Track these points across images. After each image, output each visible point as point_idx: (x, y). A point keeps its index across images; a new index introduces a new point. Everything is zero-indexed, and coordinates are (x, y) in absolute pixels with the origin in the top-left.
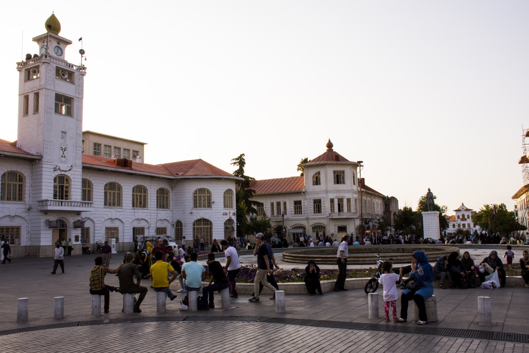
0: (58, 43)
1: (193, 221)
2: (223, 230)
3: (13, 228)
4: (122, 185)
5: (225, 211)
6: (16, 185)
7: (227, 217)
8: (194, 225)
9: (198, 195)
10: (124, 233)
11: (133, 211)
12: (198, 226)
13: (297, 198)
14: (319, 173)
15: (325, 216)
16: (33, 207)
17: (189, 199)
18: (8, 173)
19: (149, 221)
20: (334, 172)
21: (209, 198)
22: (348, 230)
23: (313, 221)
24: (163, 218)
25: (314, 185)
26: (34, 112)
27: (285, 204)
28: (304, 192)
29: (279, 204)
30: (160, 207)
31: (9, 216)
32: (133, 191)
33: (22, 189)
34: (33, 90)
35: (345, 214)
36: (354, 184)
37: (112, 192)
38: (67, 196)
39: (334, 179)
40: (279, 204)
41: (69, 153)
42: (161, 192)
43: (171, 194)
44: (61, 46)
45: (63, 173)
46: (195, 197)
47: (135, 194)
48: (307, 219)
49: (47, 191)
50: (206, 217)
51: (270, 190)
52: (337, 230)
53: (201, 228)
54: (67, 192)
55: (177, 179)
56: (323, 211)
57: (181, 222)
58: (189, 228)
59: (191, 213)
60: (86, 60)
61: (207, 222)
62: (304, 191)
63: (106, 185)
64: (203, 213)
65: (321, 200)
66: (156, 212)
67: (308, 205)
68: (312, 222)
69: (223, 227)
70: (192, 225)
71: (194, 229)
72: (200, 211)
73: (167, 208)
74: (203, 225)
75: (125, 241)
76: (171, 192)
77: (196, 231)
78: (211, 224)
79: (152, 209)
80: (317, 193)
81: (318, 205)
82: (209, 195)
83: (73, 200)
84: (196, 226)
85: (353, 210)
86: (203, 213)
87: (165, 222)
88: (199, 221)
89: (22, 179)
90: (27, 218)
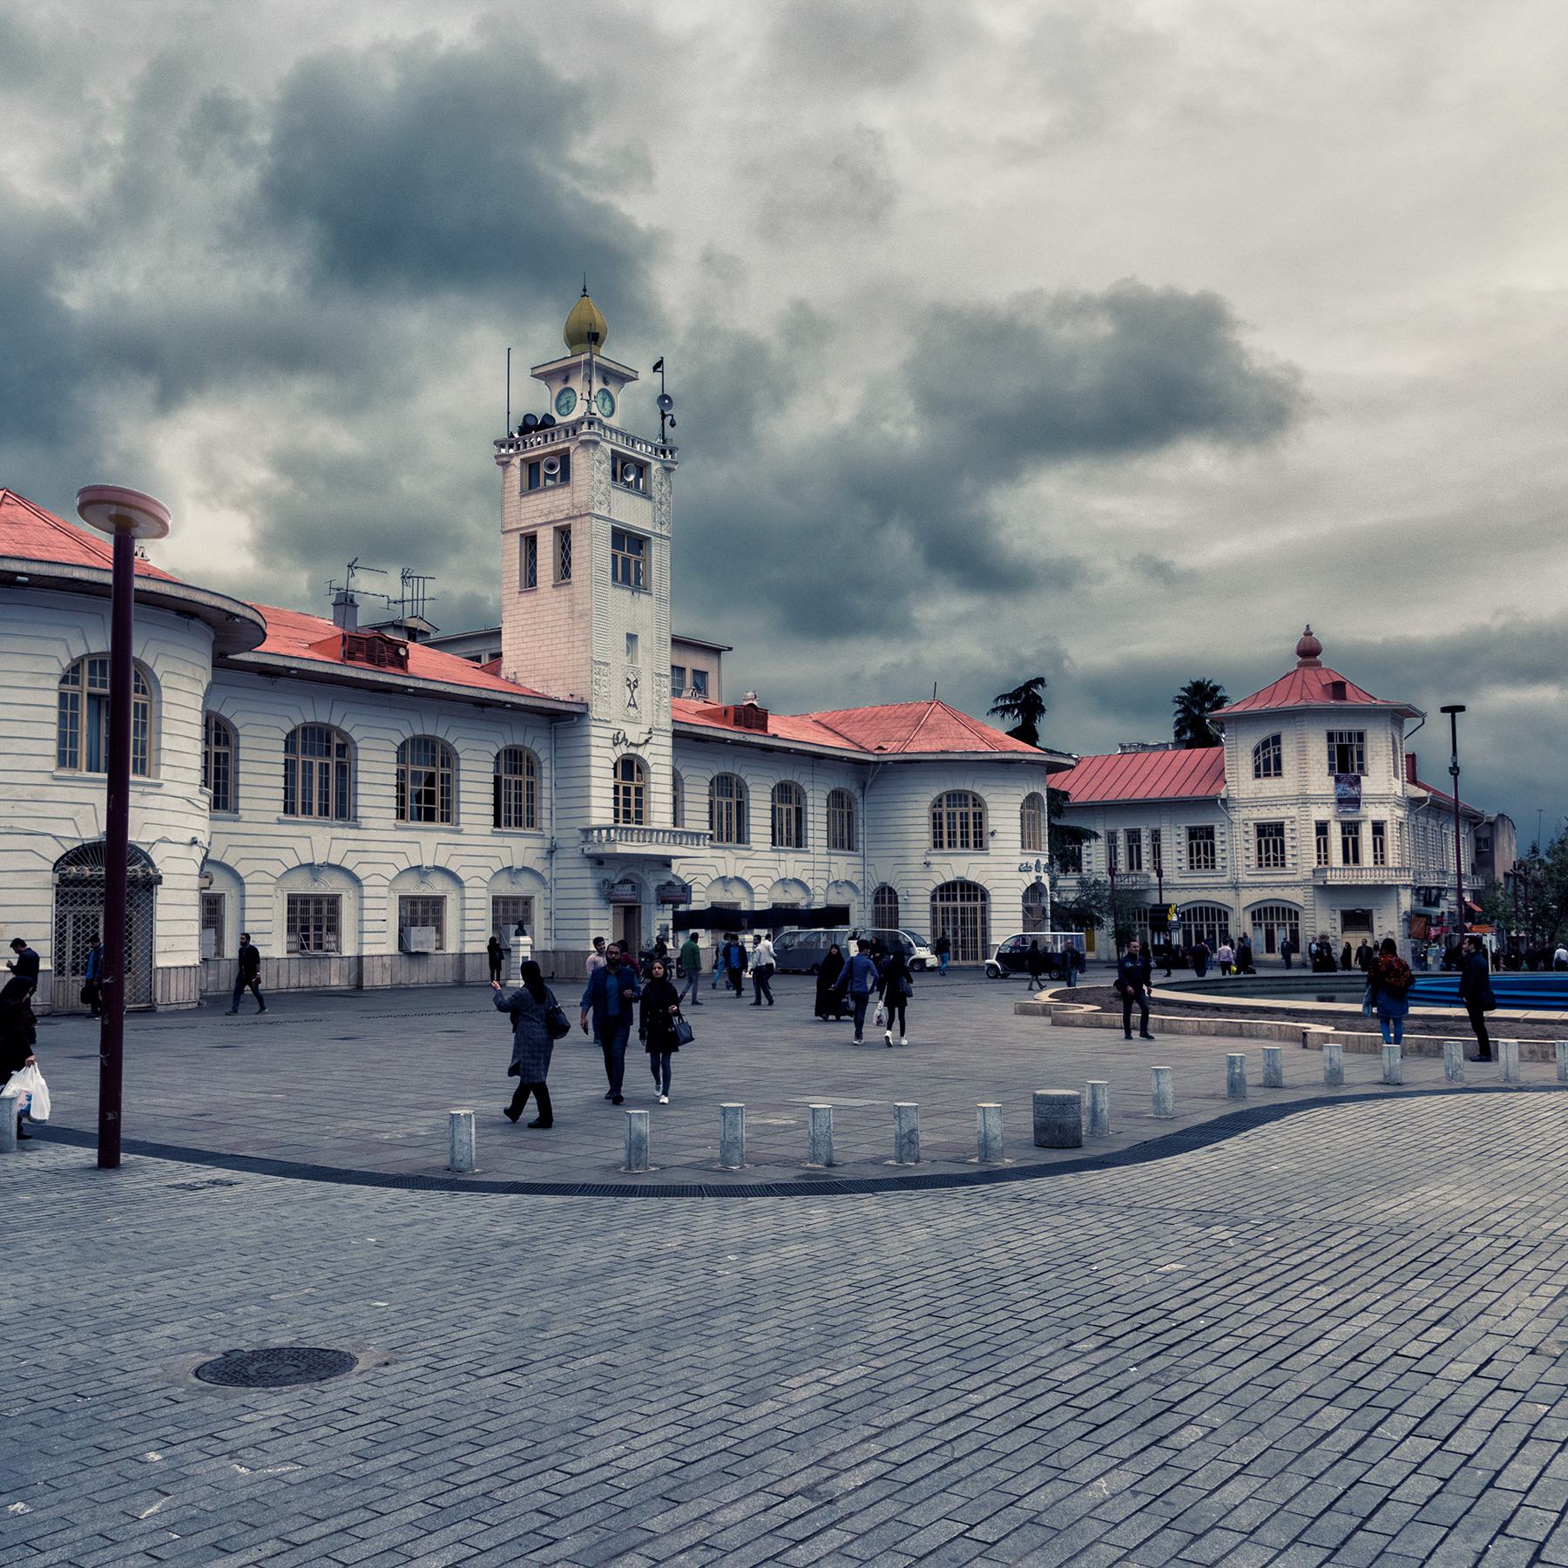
0: (606, 382)
1: (932, 887)
2: (1020, 916)
3: (318, 899)
4: (458, 747)
5: (1025, 860)
6: (433, 774)
7: (1030, 879)
8: (933, 898)
9: (945, 810)
10: (361, 920)
11: (774, 856)
12: (945, 904)
13: (1201, 821)
14: (1277, 740)
15: (1297, 878)
16: (561, 844)
17: (920, 821)
18: (304, 729)
19: (810, 884)
20: (1330, 736)
21: (979, 818)
22: (1376, 924)
23: (1256, 891)
24: (518, 865)
25: (1258, 776)
26: (556, 580)
27: (1156, 836)
28: (1224, 801)
29: (1134, 837)
30: (835, 846)
31: (311, 865)
32: (401, 759)
33: (226, 772)
34: (551, 518)
35: (1367, 872)
36: (1396, 775)
37: (316, 762)
38: (639, 814)
39: (1331, 757)
40: (1134, 837)
41: (645, 695)
42: (513, 761)
43: (546, 773)
44: (611, 388)
45: (632, 750)
46: (937, 818)
47: (623, 784)
48: (1236, 887)
49: (601, 810)
50: (971, 877)
51: (1107, 784)
52: (1338, 924)
53: (955, 910)
54: (639, 803)
55: (885, 763)
56: (1289, 861)
57: (890, 889)
58: (919, 907)
59: (927, 864)
60: (673, 424)
61: (972, 890)
62: (1224, 796)
63: (291, 736)
64: (960, 866)
65: (1282, 824)
66: (826, 859)
67: (1237, 847)
68: (1250, 897)
69: (1020, 908)
70: (928, 899)
71: (934, 910)
72: (951, 860)
73: (531, 824)
74: (962, 899)
75: (469, 949)
76: (545, 764)
77: (939, 915)
78: (985, 895)
79: (818, 850)
80: (1271, 802)
81: (1271, 836)
82: (977, 809)
83: (655, 826)
84: (939, 904)
85: (1392, 858)
86: (960, 866)
87: (846, 890)
88: (947, 890)
89: (226, 737)
90: (546, 875)
